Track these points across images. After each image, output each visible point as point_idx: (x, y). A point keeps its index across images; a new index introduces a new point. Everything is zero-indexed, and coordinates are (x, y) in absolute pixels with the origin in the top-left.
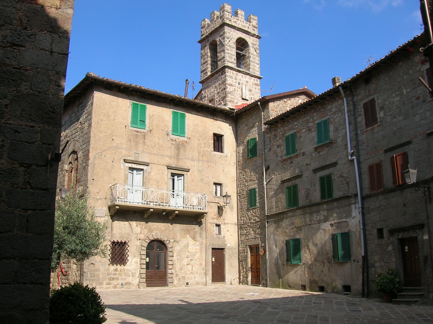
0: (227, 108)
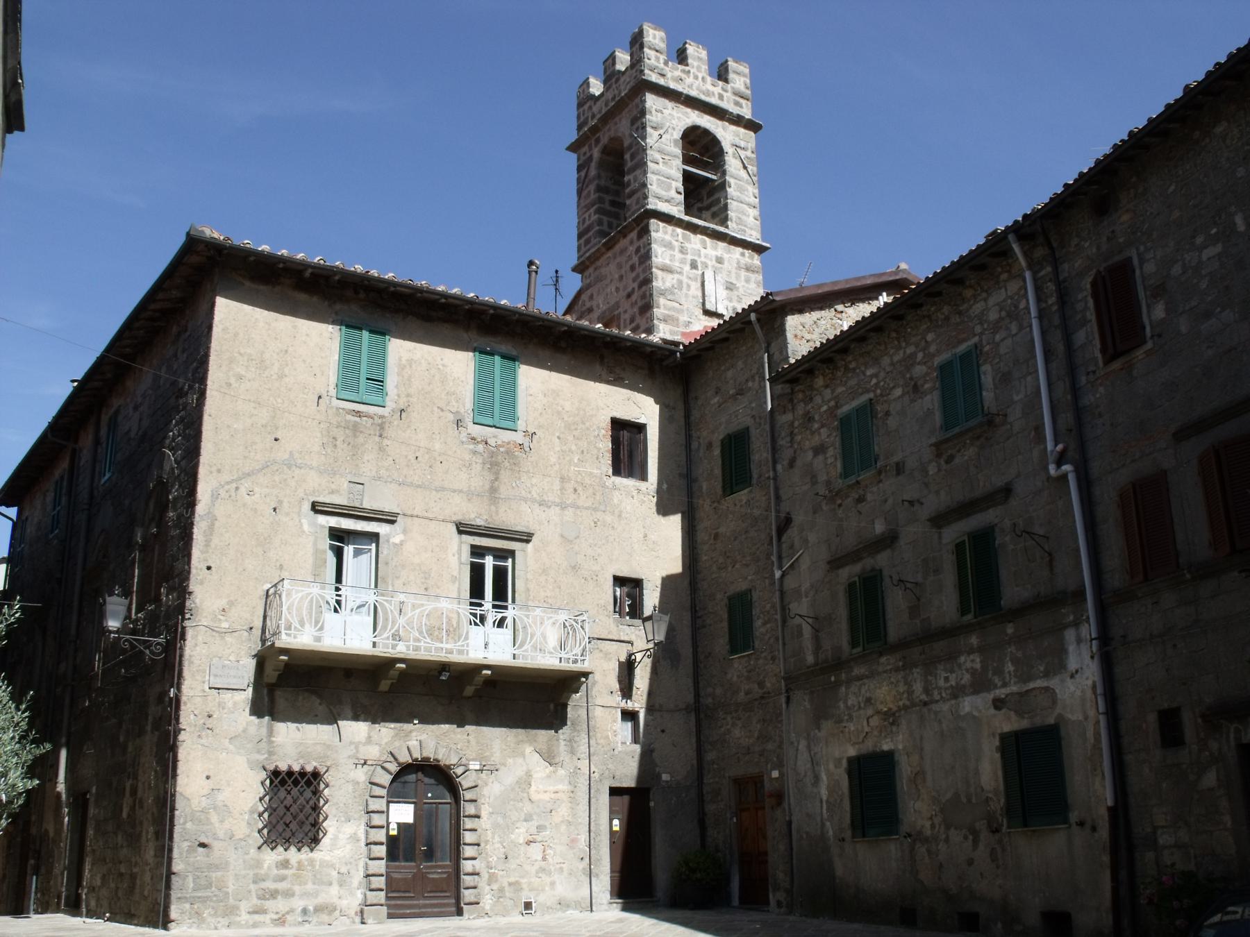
0: (655, 339)
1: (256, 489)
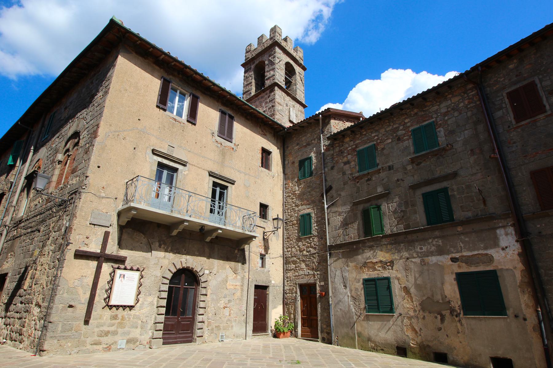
1: (127, 138)
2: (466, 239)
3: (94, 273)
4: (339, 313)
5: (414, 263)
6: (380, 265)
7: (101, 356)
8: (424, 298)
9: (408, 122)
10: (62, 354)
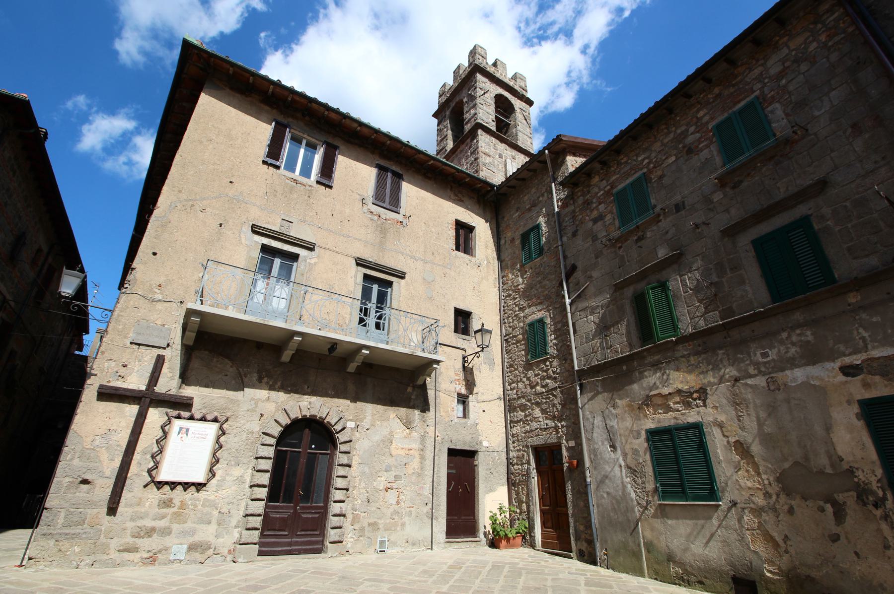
2: (874, 319)
3: (132, 425)
4: (606, 501)
5: (754, 387)
6: (677, 399)
7: (135, 574)
8: (786, 465)
9: (705, 115)
10: (61, 567)
